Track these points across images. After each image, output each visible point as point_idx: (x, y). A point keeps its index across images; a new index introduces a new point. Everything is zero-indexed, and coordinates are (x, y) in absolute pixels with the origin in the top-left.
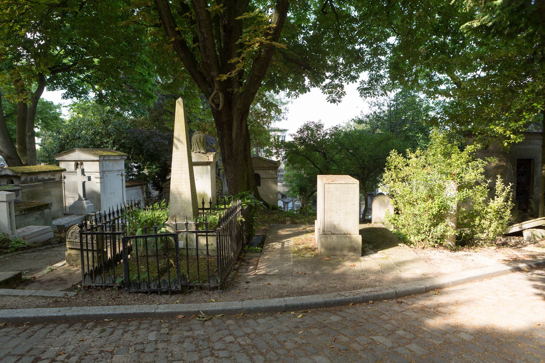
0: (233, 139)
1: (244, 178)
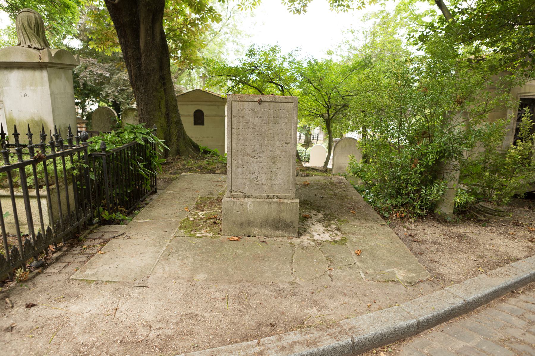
0: (142, 51)
1: (160, 108)
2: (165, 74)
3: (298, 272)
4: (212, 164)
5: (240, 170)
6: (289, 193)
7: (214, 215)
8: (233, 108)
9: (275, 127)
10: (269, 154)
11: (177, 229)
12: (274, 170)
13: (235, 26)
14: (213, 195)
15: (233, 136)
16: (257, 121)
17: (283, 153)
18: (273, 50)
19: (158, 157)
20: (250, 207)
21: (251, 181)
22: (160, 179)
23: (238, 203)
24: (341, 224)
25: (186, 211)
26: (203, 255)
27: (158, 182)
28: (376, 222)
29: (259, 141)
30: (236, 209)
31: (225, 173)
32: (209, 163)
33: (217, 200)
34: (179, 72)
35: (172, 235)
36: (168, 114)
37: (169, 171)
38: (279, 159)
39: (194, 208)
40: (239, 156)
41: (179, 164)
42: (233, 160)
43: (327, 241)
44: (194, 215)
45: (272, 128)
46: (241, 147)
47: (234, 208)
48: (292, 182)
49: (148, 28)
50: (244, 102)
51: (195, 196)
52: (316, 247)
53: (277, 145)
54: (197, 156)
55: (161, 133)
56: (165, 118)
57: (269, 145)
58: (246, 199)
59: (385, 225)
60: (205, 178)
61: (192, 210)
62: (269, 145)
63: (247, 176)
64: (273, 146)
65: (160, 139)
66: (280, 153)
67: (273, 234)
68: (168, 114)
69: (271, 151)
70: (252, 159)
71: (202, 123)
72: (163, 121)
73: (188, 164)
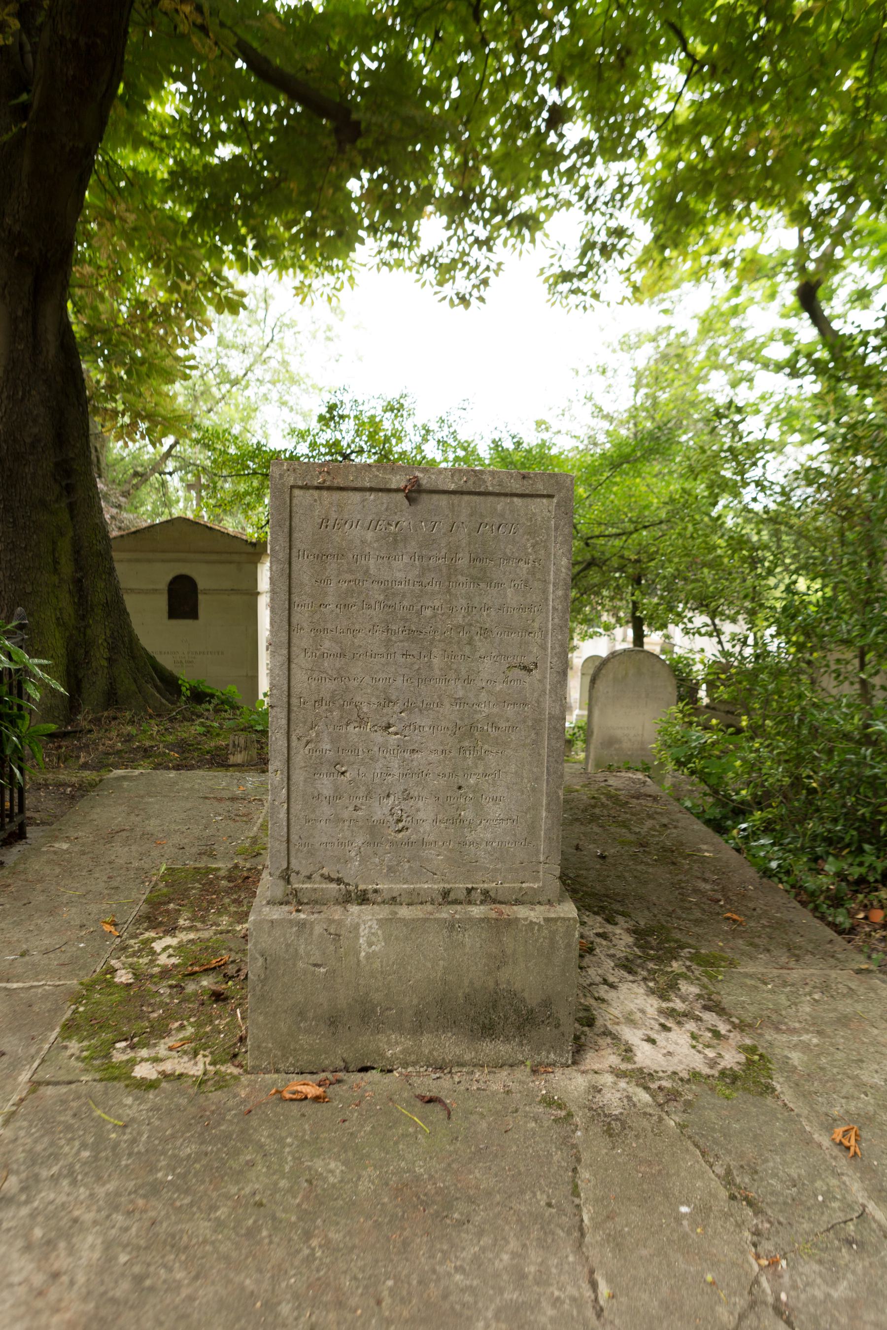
1: (56, 562)
2: (72, 459)
3: (624, 1299)
4: (218, 735)
5: (325, 786)
6: (536, 879)
7: (215, 952)
8: (296, 520)
9: (476, 602)
10: (449, 713)
11: (54, 1034)
12: (472, 781)
13: (284, 363)
14: (212, 856)
15: (294, 640)
16: (399, 575)
17: (510, 711)
18: (395, 408)
19: (27, 717)
20: (370, 944)
21: (374, 831)
22: (46, 786)
23: (318, 930)
24: (711, 977)
25: (106, 936)
26: (157, 1208)
27: (30, 801)
28: (832, 961)
29: (410, 660)
30: (308, 954)
31: (261, 764)
32: (208, 733)
33: (230, 879)
34: (135, 481)
35: (24, 1077)
36: (80, 581)
37: (78, 757)
38: (494, 733)
39: (138, 921)
40: (321, 726)
41: (114, 734)
42: (294, 743)
43: (695, 1075)
44: (134, 955)
45: (463, 602)
46: (330, 685)
47: (301, 951)
48: (548, 830)
49: (20, 313)
50: (345, 494)
51: (146, 864)
52: (661, 1119)
53: (485, 675)
54: (173, 710)
55: (56, 640)
56: (70, 592)
57: (452, 675)
58: (354, 909)
59: (868, 971)
60: (192, 788)
61: (132, 929)
62: (452, 675)
63: (356, 809)
64: (468, 680)
65: (31, 657)
66: (495, 710)
67: (467, 1057)
68: (80, 581)
69: (458, 701)
70: (379, 737)
71: (193, 614)
72: (65, 601)
73: (141, 737)
